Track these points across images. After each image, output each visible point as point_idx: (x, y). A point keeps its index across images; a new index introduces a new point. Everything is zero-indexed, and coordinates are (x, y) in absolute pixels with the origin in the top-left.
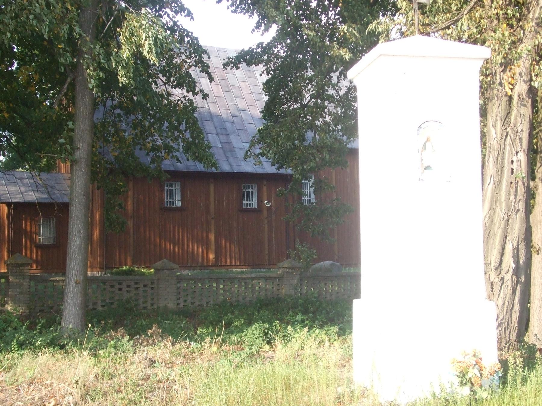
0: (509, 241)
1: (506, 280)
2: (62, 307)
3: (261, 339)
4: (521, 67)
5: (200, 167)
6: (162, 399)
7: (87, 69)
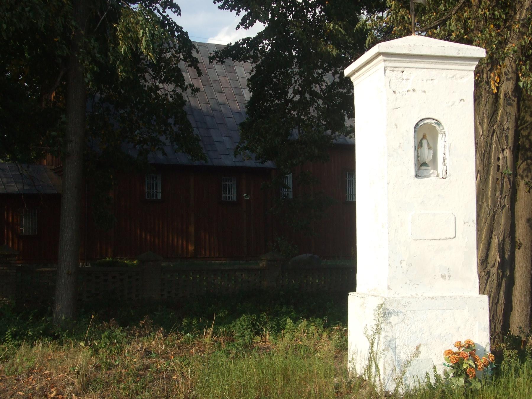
0: (495, 236)
1: (491, 274)
2: (54, 298)
3: (249, 330)
5: (184, 159)
6: (164, 389)
7: (82, 63)
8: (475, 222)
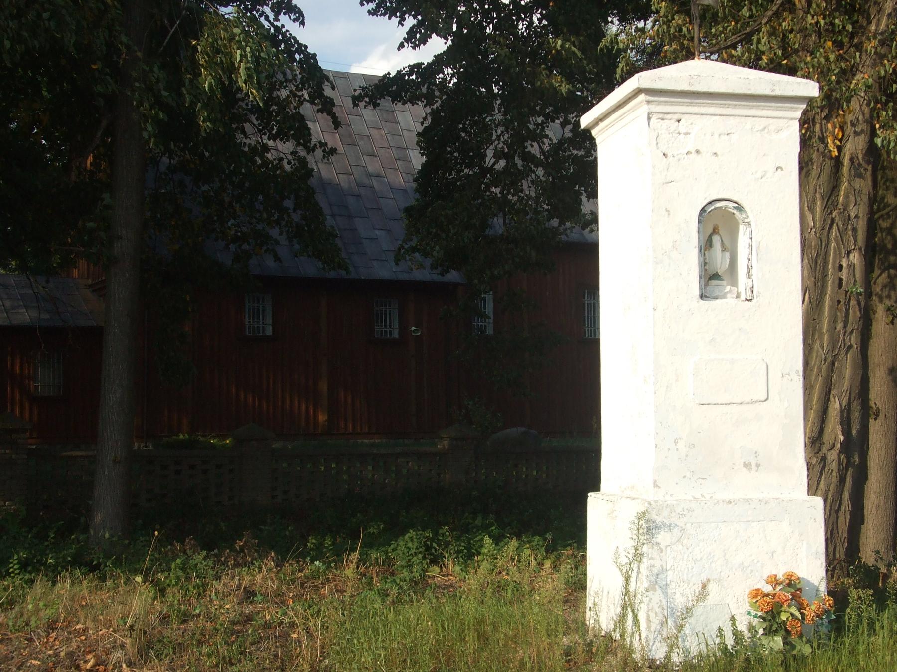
0: (834, 397)
1: (829, 461)
2: (90, 502)
3: (420, 556)
4: (857, 108)
5: (309, 268)
6: (276, 656)
7: (138, 107)
8: (801, 373)
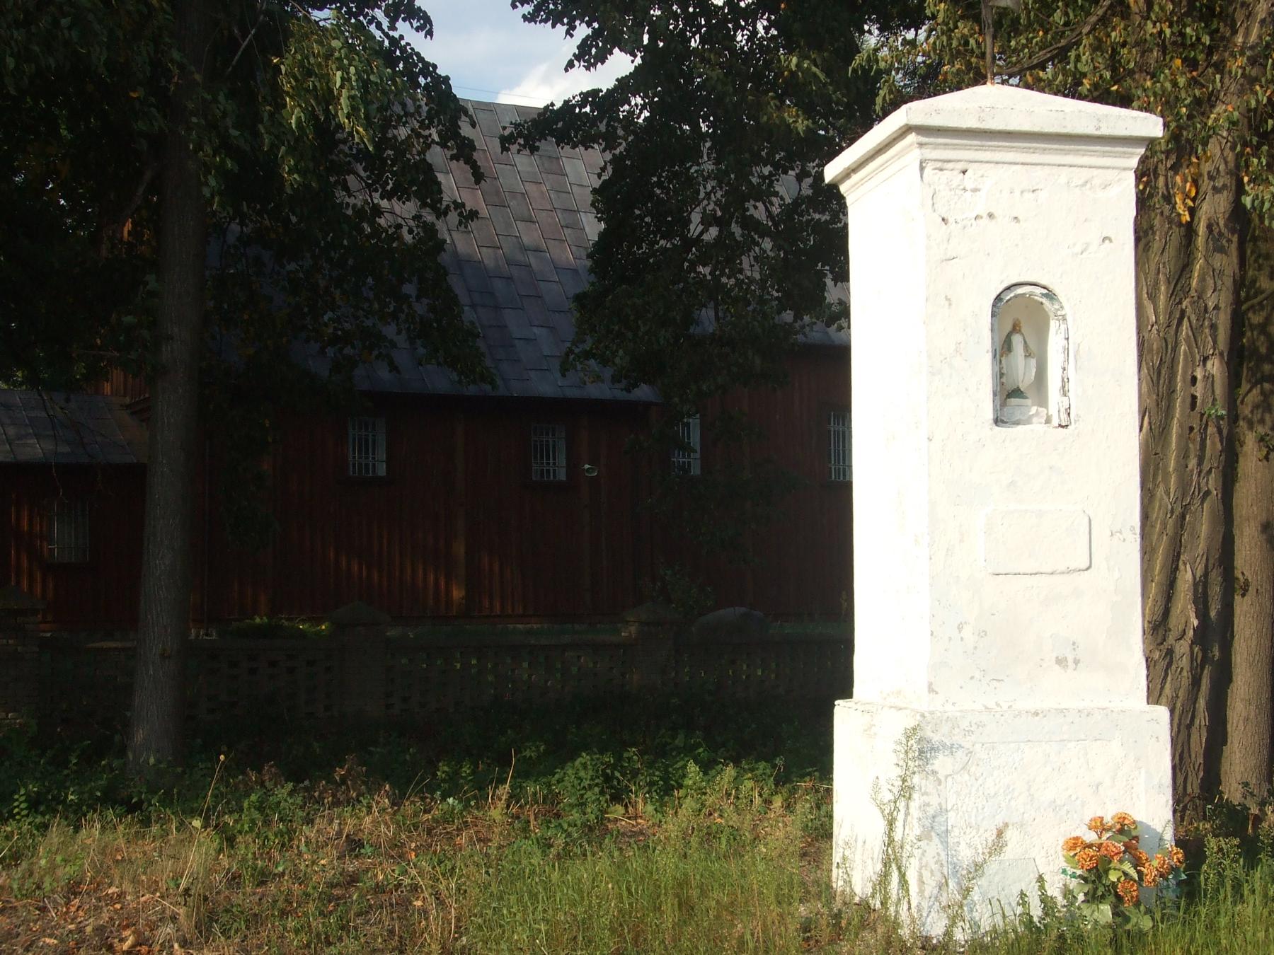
0: (1185, 564)
1: (1177, 655)
2: (128, 714)
3: (597, 790)
5: (440, 380)
7: (196, 151)
8: (1138, 530)
